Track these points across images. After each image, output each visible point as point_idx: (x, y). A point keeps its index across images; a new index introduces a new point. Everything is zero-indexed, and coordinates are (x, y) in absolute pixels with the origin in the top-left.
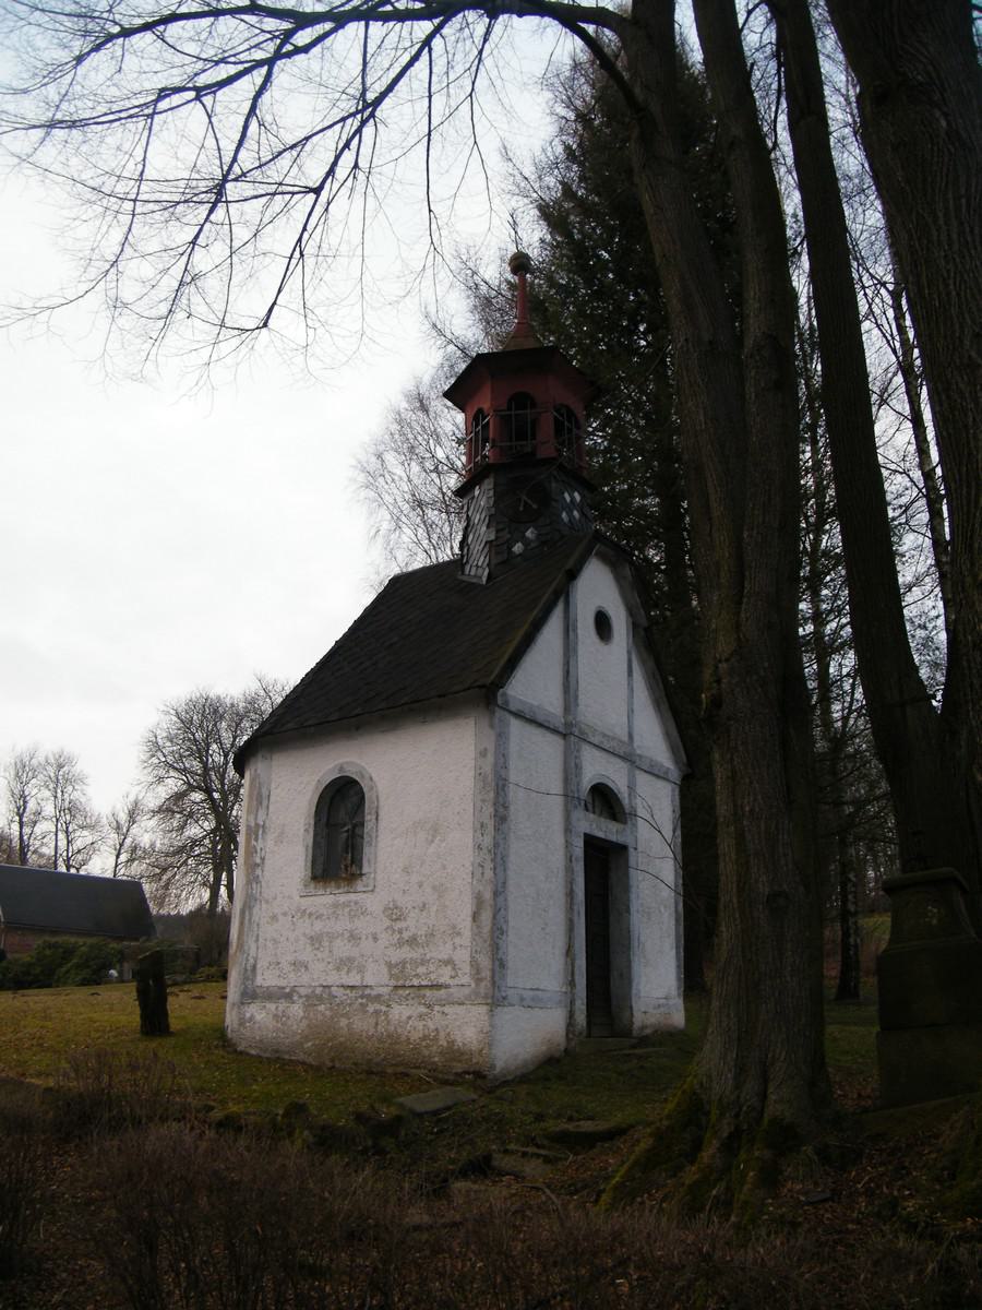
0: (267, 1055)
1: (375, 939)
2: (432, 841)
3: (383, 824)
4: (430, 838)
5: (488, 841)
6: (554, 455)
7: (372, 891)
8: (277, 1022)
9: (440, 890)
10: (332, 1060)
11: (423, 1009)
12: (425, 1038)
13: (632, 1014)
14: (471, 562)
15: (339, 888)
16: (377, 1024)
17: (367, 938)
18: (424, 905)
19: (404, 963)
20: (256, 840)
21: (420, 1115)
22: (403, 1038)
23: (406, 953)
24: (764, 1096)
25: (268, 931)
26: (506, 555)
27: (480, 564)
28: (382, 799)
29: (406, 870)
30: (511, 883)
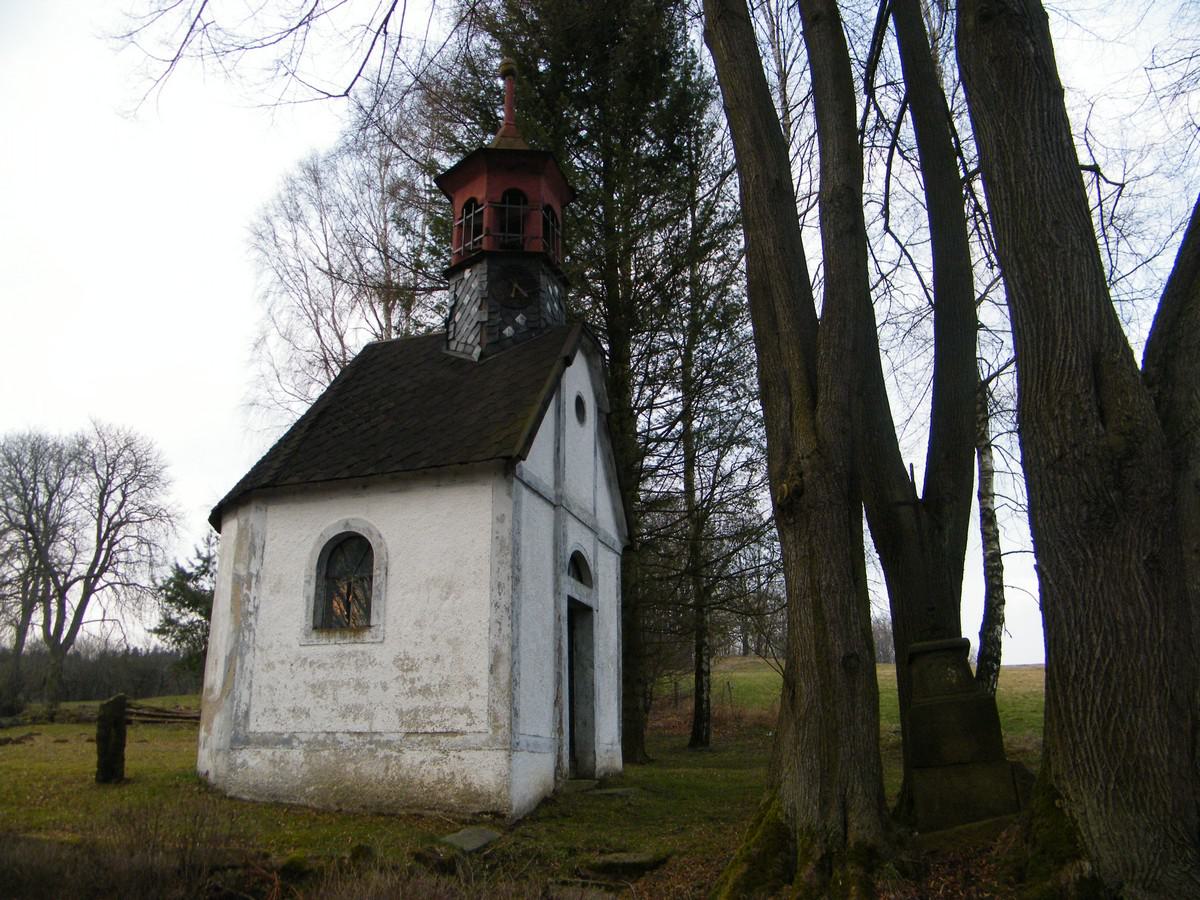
0: (264, 799)
1: (385, 687)
2: (447, 598)
3: (391, 580)
4: (444, 594)
5: (505, 600)
6: (541, 249)
7: (381, 642)
8: (275, 767)
9: (454, 643)
10: (338, 804)
11: (437, 754)
12: (439, 781)
13: (595, 759)
14: (458, 338)
15: (345, 638)
16: (387, 768)
17: (376, 687)
18: (438, 657)
19: (416, 711)
20: (249, 588)
21: (470, 853)
22: (416, 781)
23: (418, 701)
24: (845, 824)
25: (262, 678)
26: (497, 337)
27: (469, 342)
28: (391, 556)
29: (419, 624)
30: (522, 638)
